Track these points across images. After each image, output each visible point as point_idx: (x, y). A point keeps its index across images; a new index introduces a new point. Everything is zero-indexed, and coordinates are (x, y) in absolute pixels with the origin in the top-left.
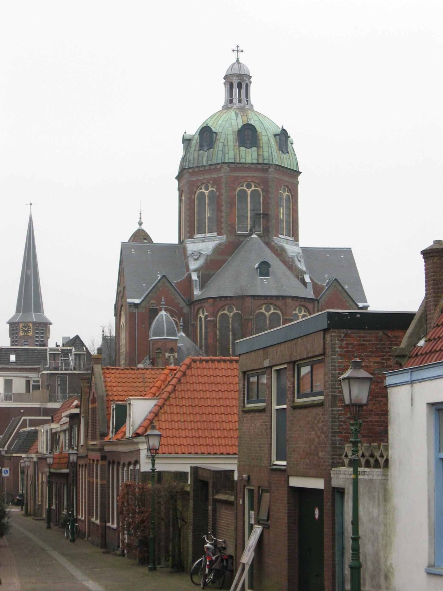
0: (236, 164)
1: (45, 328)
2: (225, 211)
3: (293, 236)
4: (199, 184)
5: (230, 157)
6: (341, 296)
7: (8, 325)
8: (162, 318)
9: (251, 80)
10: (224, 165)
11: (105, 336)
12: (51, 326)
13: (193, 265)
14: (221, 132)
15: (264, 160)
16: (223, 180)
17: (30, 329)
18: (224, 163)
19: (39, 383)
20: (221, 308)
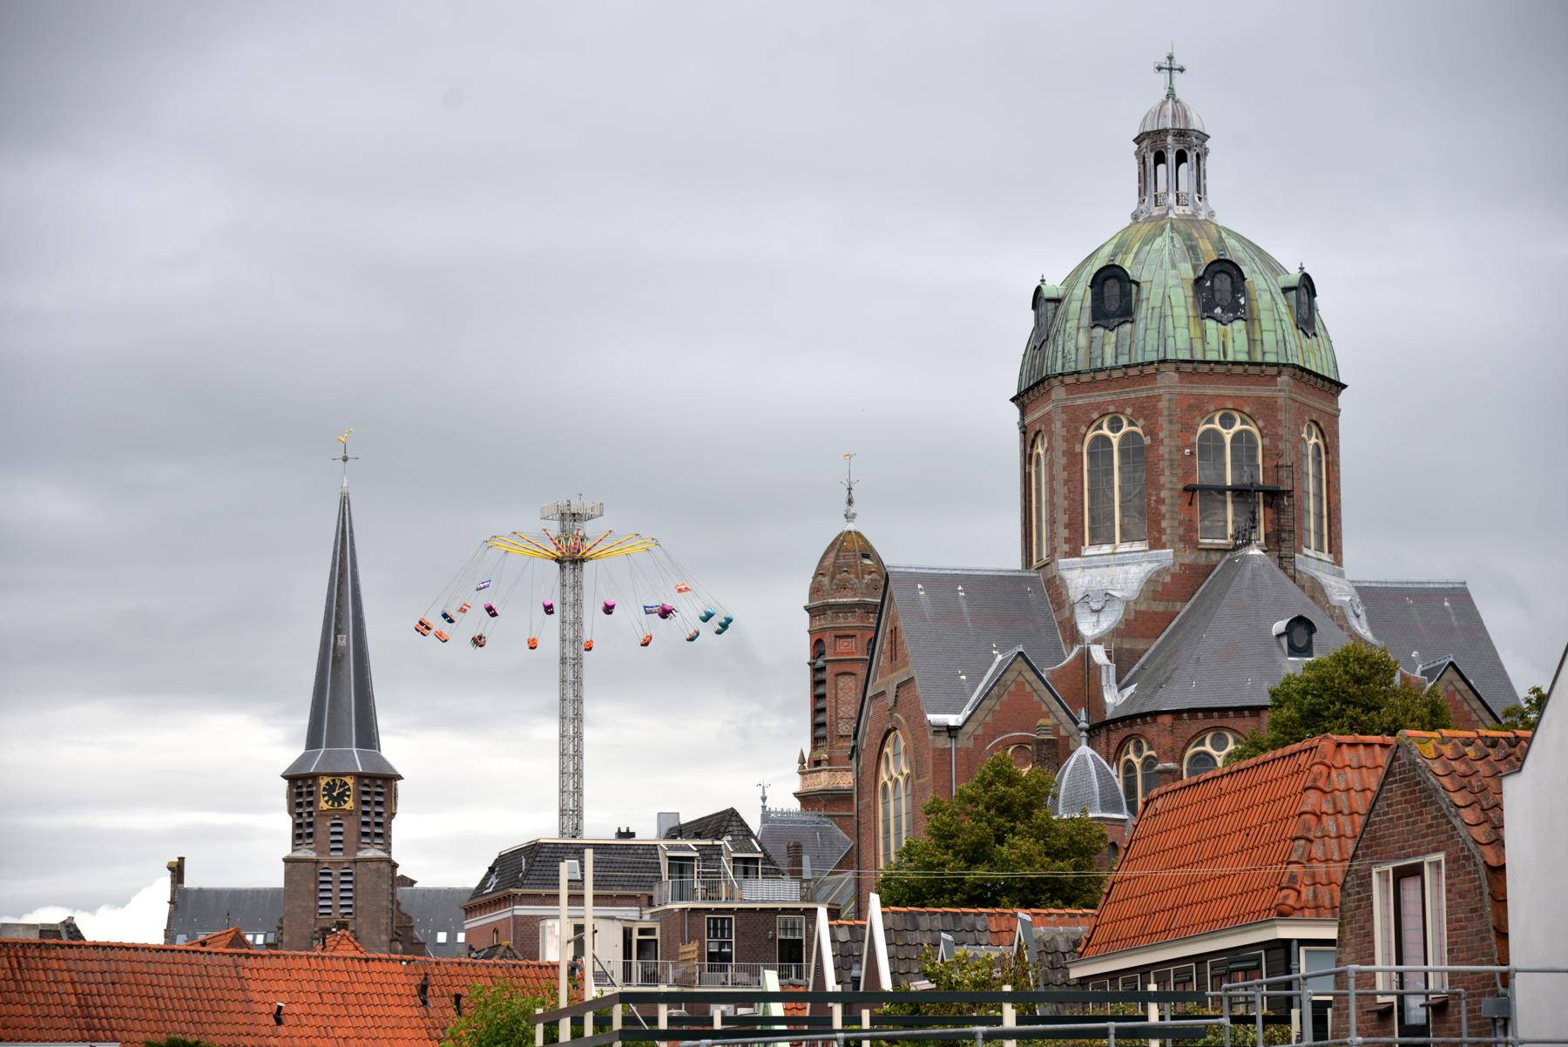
0: (1195, 364)
1: (385, 790)
2: (1168, 485)
3: (1330, 552)
4: (1095, 416)
5: (1179, 347)
6: (1466, 707)
7: (285, 783)
8: (1086, 762)
9: (1208, 144)
10: (1163, 367)
11: (770, 812)
12: (398, 782)
13: (1088, 627)
14: (1151, 281)
15: (1264, 354)
16: (1163, 405)
17: (347, 793)
18: (1164, 361)
19: (654, 934)
20: (1194, 737)
